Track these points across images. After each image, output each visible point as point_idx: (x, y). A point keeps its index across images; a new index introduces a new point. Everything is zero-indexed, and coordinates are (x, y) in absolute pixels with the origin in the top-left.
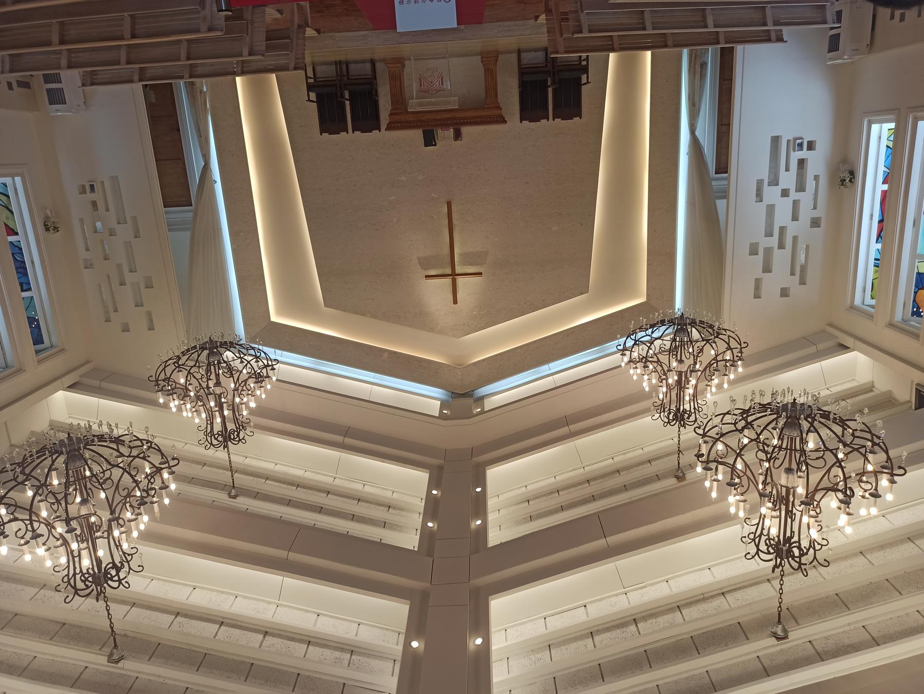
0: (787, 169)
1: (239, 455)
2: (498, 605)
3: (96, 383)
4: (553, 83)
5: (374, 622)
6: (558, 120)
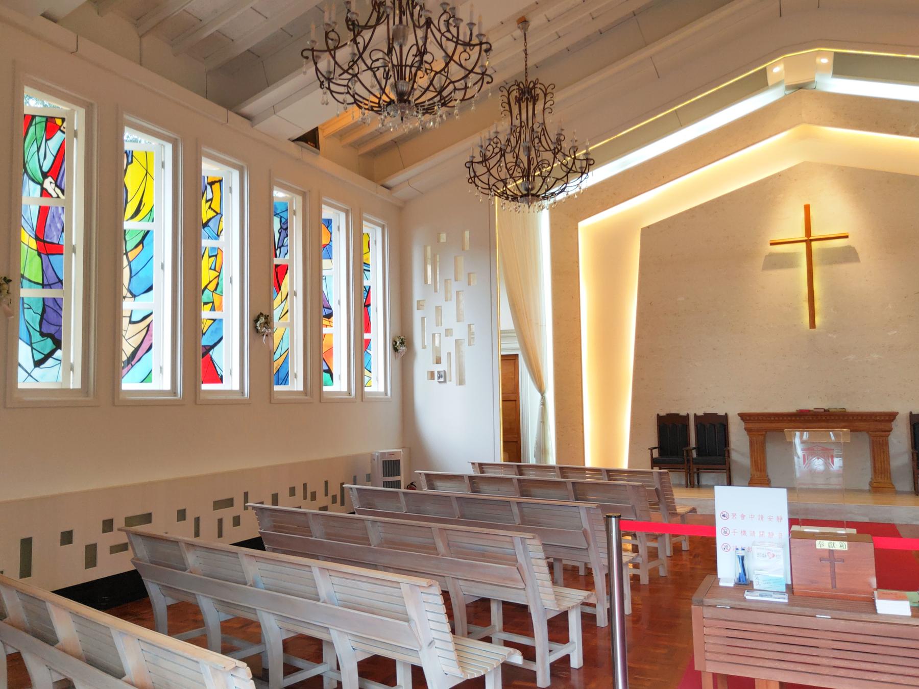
0: (449, 354)
4: (689, 452)
6: (683, 413)
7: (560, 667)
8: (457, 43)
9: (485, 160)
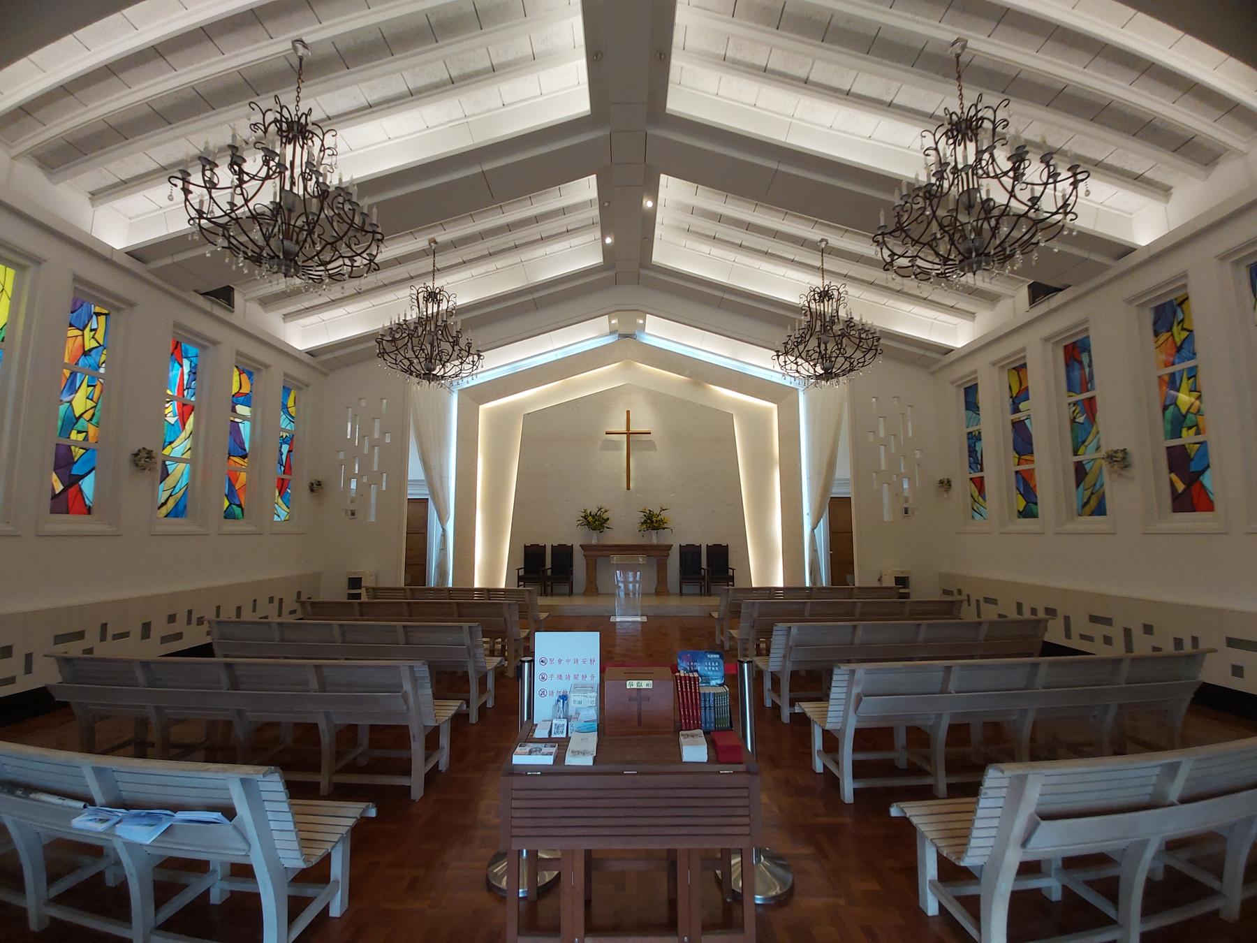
1: (817, 282)
2: (581, 105)
3: (929, 354)
4: (544, 572)
5: (703, 89)
7: (482, 709)
8: (351, 226)
9: (394, 340)
